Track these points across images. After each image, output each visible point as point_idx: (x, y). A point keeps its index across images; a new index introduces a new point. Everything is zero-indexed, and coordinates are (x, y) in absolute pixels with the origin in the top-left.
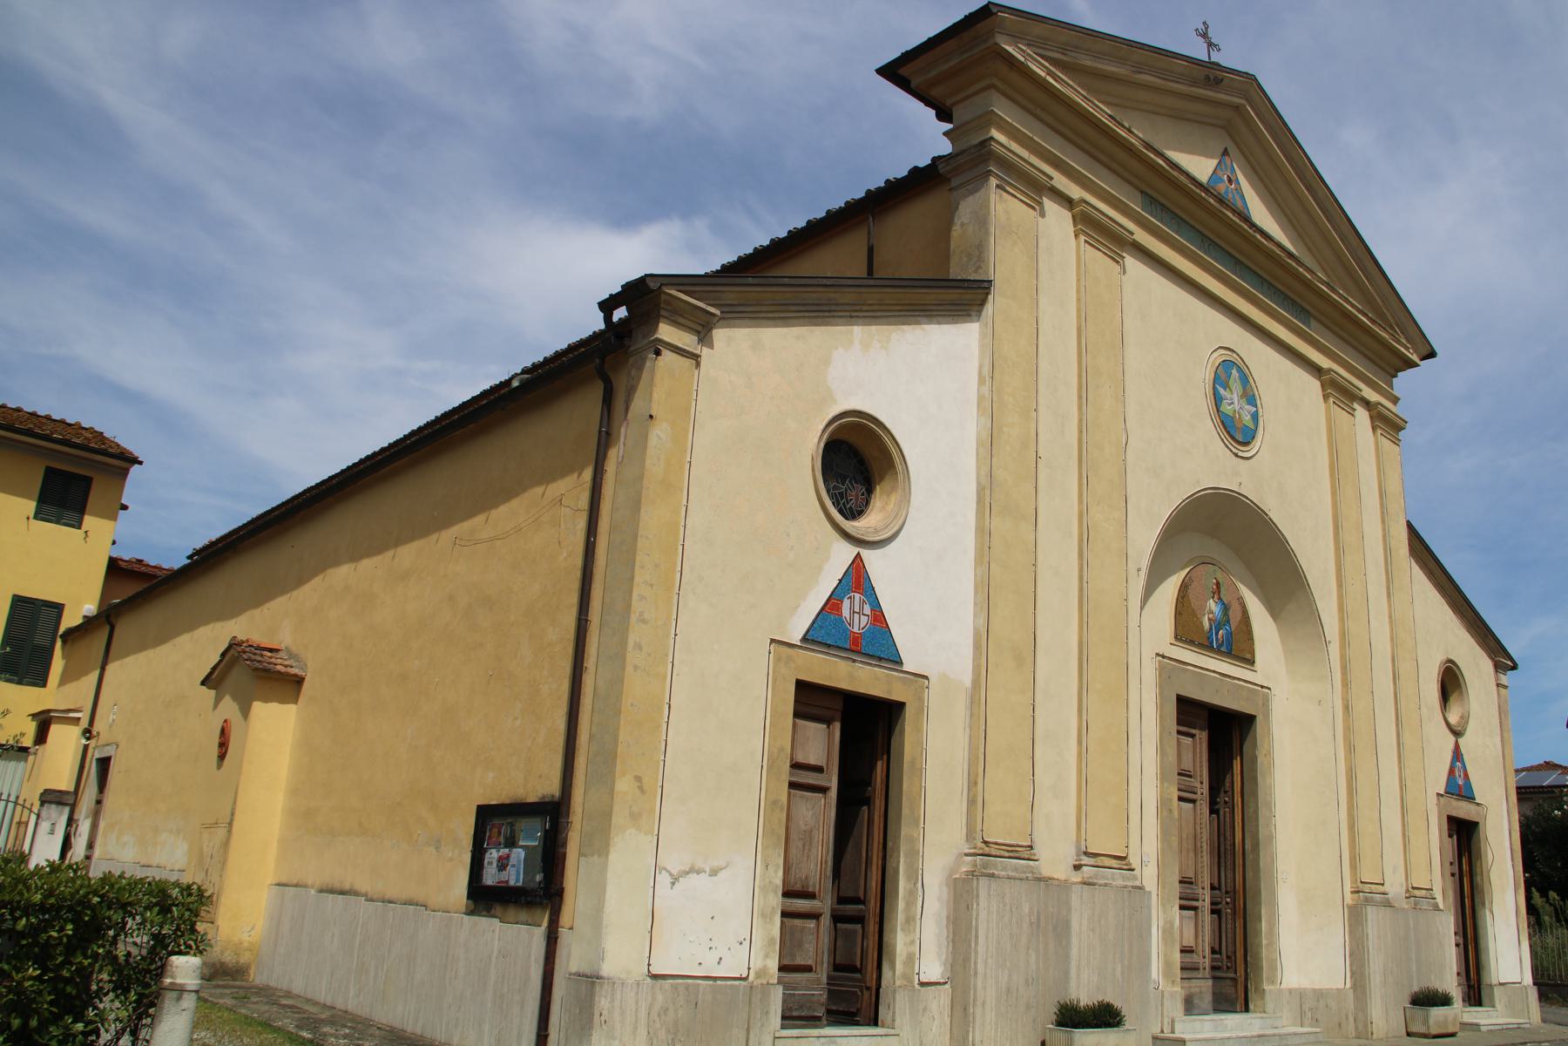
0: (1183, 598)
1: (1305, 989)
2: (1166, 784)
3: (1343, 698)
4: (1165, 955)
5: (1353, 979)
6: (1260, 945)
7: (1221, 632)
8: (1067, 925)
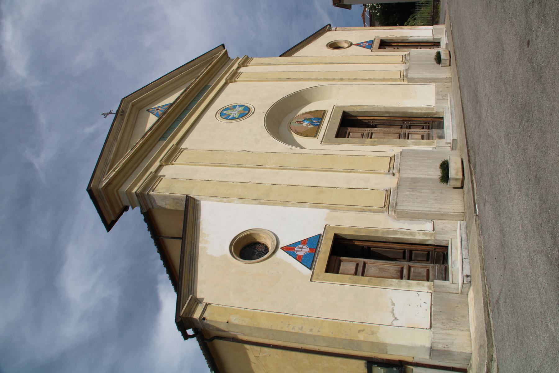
0: (301, 134)
1: (436, 98)
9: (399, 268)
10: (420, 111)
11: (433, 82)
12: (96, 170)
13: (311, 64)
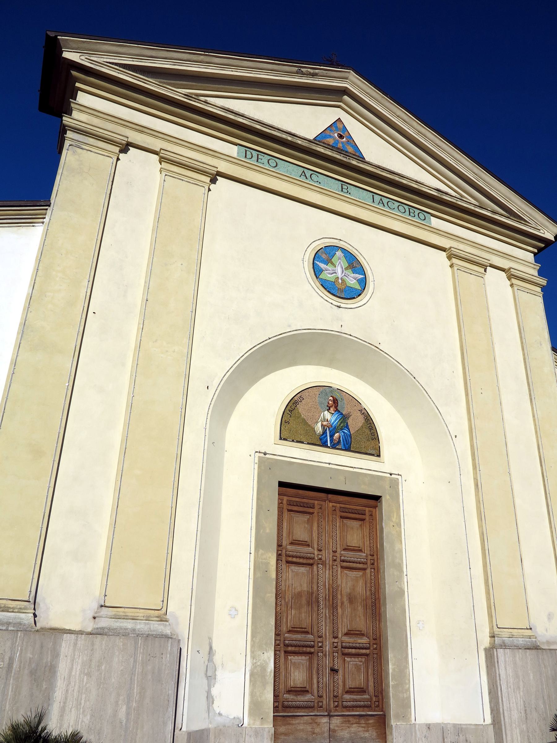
0: (291, 411)
1: (447, 724)
2: (261, 551)
3: (474, 479)
4: (252, 694)
5: (493, 715)
6: (388, 685)
7: (337, 435)
8: (52, 669)
9: (364, 631)
10: (391, 683)
11: (494, 716)
12: (271, 70)
13: (534, 416)
